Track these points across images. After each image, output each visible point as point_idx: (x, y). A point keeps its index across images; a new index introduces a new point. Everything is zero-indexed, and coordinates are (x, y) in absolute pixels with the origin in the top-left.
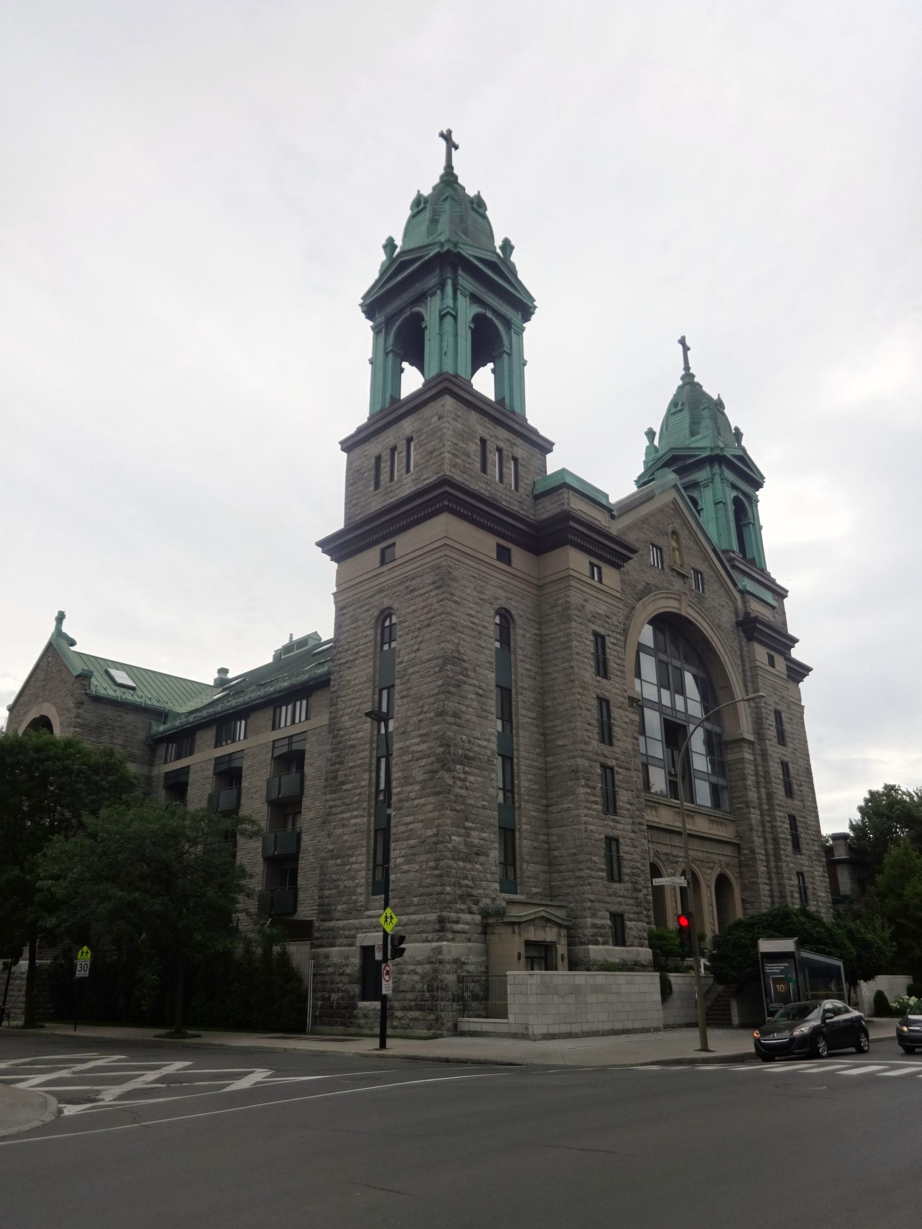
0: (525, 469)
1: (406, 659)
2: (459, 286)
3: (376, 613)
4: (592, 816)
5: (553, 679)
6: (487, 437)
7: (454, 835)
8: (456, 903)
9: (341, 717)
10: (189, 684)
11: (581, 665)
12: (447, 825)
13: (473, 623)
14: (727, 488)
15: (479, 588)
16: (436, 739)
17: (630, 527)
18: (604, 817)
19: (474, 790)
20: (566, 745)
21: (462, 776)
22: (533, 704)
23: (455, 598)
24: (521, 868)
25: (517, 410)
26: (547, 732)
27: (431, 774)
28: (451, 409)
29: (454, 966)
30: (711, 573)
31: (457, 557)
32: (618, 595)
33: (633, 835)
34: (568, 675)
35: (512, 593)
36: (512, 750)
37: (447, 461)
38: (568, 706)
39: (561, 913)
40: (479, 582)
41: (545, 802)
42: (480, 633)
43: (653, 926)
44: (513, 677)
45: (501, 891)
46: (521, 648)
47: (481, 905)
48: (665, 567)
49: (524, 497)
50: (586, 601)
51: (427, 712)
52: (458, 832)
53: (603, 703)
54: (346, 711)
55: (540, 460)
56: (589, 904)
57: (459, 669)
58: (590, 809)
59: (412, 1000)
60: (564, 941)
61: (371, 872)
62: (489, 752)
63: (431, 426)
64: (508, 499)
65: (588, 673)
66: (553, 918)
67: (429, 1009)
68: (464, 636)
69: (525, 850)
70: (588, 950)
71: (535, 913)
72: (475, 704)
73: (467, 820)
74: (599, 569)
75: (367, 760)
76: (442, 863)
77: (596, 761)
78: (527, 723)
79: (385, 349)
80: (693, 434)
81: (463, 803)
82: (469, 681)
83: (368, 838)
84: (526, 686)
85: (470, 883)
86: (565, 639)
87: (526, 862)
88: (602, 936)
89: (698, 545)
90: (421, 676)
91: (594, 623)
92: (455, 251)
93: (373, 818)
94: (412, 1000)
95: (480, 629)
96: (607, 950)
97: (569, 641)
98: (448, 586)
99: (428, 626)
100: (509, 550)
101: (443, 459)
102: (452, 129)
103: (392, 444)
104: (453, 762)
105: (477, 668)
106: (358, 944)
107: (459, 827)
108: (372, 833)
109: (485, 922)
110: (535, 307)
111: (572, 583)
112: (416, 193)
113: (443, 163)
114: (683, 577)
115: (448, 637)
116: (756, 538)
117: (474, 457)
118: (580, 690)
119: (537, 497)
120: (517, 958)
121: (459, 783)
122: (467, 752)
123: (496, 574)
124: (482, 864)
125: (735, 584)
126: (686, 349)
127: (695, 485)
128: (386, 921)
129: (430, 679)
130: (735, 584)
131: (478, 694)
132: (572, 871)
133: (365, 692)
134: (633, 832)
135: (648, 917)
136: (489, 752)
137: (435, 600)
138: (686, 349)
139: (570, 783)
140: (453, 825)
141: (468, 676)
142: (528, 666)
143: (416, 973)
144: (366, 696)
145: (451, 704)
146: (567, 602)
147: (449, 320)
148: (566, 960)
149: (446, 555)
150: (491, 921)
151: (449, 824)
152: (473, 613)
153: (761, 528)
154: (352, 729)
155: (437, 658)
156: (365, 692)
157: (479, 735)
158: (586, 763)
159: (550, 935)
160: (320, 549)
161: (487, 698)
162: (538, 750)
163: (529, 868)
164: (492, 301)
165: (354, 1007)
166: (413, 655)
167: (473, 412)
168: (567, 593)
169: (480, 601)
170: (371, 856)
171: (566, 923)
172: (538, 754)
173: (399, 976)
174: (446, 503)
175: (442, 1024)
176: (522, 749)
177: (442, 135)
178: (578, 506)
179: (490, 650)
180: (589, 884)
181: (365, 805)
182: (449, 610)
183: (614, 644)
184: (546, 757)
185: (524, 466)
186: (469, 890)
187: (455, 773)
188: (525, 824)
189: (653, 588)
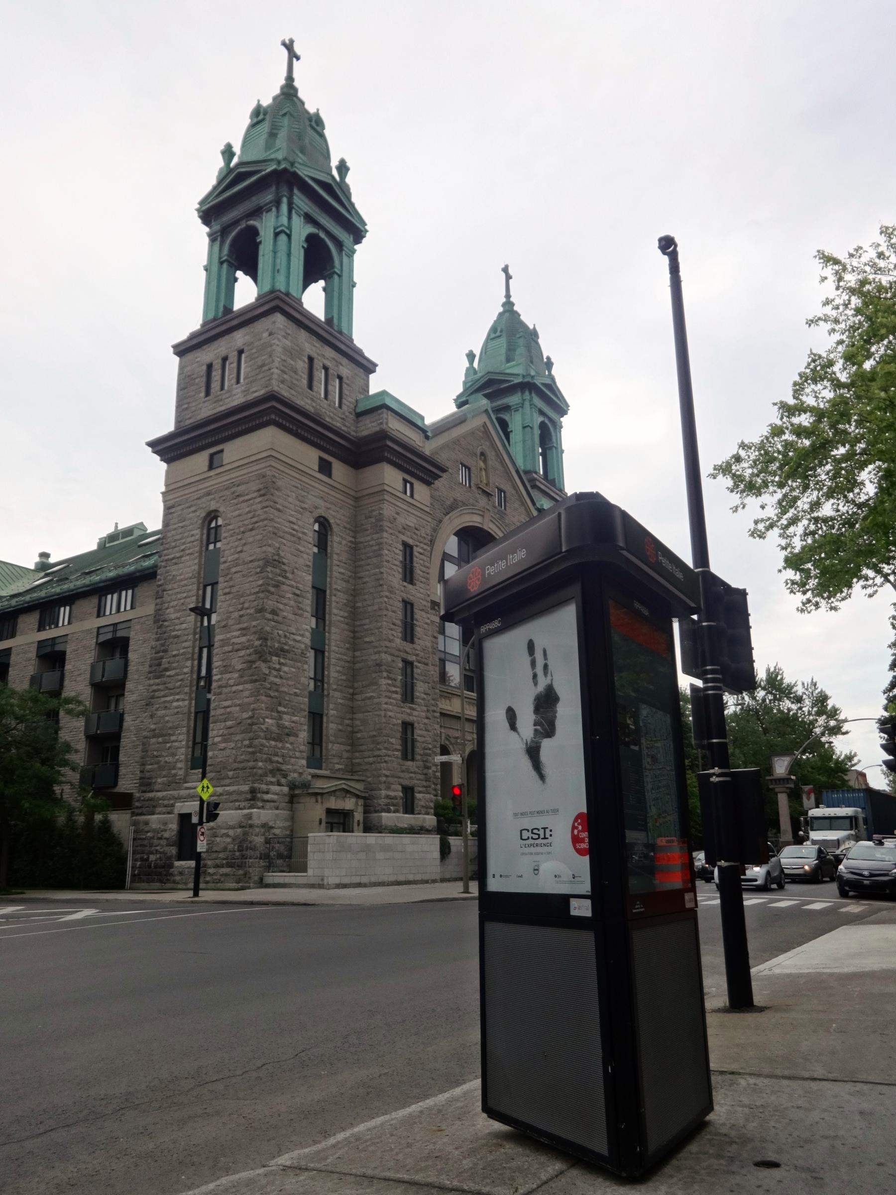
0: (349, 388)
1: (230, 559)
2: (294, 206)
3: (203, 515)
4: (391, 704)
5: (364, 583)
6: (314, 355)
7: (267, 718)
8: (267, 776)
9: (167, 608)
11: (389, 571)
12: (262, 709)
14: (534, 414)
15: (300, 498)
16: (255, 633)
17: (442, 448)
18: (402, 705)
19: (287, 679)
20: (372, 642)
21: (278, 666)
22: (345, 604)
23: (278, 506)
24: (327, 746)
25: (345, 330)
28: (282, 327)
29: (263, 830)
30: (514, 492)
31: (282, 468)
32: (428, 509)
33: (426, 721)
34: (378, 580)
36: (325, 644)
37: (275, 376)
38: (375, 607)
39: (360, 786)
40: (301, 492)
41: (351, 691)
42: (299, 538)
43: (440, 798)
44: (328, 579)
45: (308, 767)
46: (337, 554)
47: (289, 778)
48: (472, 484)
49: (347, 414)
50: (398, 514)
51: (247, 609)
52: (271, 715)
53: (408, 606)
54: (172, 604)
55: (363, 379)
56: (384, 779)
57: (278, 571)
58: (390, 698)
59: (224, 859)
60: (360, 809)
61: (190, 750)
62: (303, 646)
63: (262, 342)
64: (332, 415)
65: (394, 577)
66: (352, 790)
67: (238, 866)
68: (285, 542)
69: (331, 732)
70: (381, 817)
71: (336, 785)
73: (280, 705)
75: (190, 650)
76: (256, 742)
77: (397, 656)
78: (338, 621)
79: (220, 258)
80: (508, 360)
81: (277, 691)
82: (288, 582)
83: (189, 719)
84: (339, 588)
85: (280, 760)
86: (376, 548)
87: (331, 742)
88: (394, 805)
89: (503, 467)
90: (244, 576)
91: (403, 534)
92: (292, 170)
93: (193, 702)
94: (224, 859)
95: (300, 535)
96: (398, 818)
97: (381, 549)
98: (272, 495)
99: (252, 530)
100: (330, 464)
101: (272, 374)
102: (294, 39)
103: (223, 354)
104: (270, 653)
105: (295, 571)
106: (176, 811)
107: (272, 711)
108: (193, 715)
109: (292, 793)
110: (367, 231)
111: (386, 497)
112: (256, 102)
113: (284, 73)
114: (488, 495)
115: (270, 542)
118: (387, 594)
119: (359, 415)
120: (318, 823)
122: (283, 646)
123: (317, 485)
124: (292, 744)
125: (534, 503)
126: (508, 277)
127: (507, 408)
128: (203, 790)
129: (251, 579)
130: (534, 503)
131: (295, 594)
132: (372, 750)
133: (190, 587)
134: (427, 718)
135: (435, 790)
136: (303, 646)
137: (259, 506)
138: (508, 277)
139: (374, 675)
141: (286, 578)
142: (342, 571)
143: (228, 836)
144: (190, 591)
145: (270, 602)
147: (283, 238)
148: (361, 825)
149: (271, 466)
150: (297, 792)
151: (264, 708)
153: (562, 451)
154: (176, 621)
156: (190, 587)
157: (294, 631)
158: (389, 658)
159: (348, 804)
160: (150, 449)
161: (304, 597)
162: (347, 645)
163: (334, 748)
164: (325, 222)
165: (171, 866)
166: (236, 556)
167: (302, 331)
168: (381, 506)
169: (301, 510)
170: (191, 735)
171: (363, 795)
172: (348, 649)
173: (213, 839)
174: (273, 417)
176: (333, 644)
177: (284, 44)
178: (395, 426)
179: (308, 554)
180: (385, 762)
181: (187, 690)
182: (272, 516)
183: (421, 554)
185: (348, 385)
186: (279, 765)
187: (271, 664)
188: (332, 710)
189: (460, 504)
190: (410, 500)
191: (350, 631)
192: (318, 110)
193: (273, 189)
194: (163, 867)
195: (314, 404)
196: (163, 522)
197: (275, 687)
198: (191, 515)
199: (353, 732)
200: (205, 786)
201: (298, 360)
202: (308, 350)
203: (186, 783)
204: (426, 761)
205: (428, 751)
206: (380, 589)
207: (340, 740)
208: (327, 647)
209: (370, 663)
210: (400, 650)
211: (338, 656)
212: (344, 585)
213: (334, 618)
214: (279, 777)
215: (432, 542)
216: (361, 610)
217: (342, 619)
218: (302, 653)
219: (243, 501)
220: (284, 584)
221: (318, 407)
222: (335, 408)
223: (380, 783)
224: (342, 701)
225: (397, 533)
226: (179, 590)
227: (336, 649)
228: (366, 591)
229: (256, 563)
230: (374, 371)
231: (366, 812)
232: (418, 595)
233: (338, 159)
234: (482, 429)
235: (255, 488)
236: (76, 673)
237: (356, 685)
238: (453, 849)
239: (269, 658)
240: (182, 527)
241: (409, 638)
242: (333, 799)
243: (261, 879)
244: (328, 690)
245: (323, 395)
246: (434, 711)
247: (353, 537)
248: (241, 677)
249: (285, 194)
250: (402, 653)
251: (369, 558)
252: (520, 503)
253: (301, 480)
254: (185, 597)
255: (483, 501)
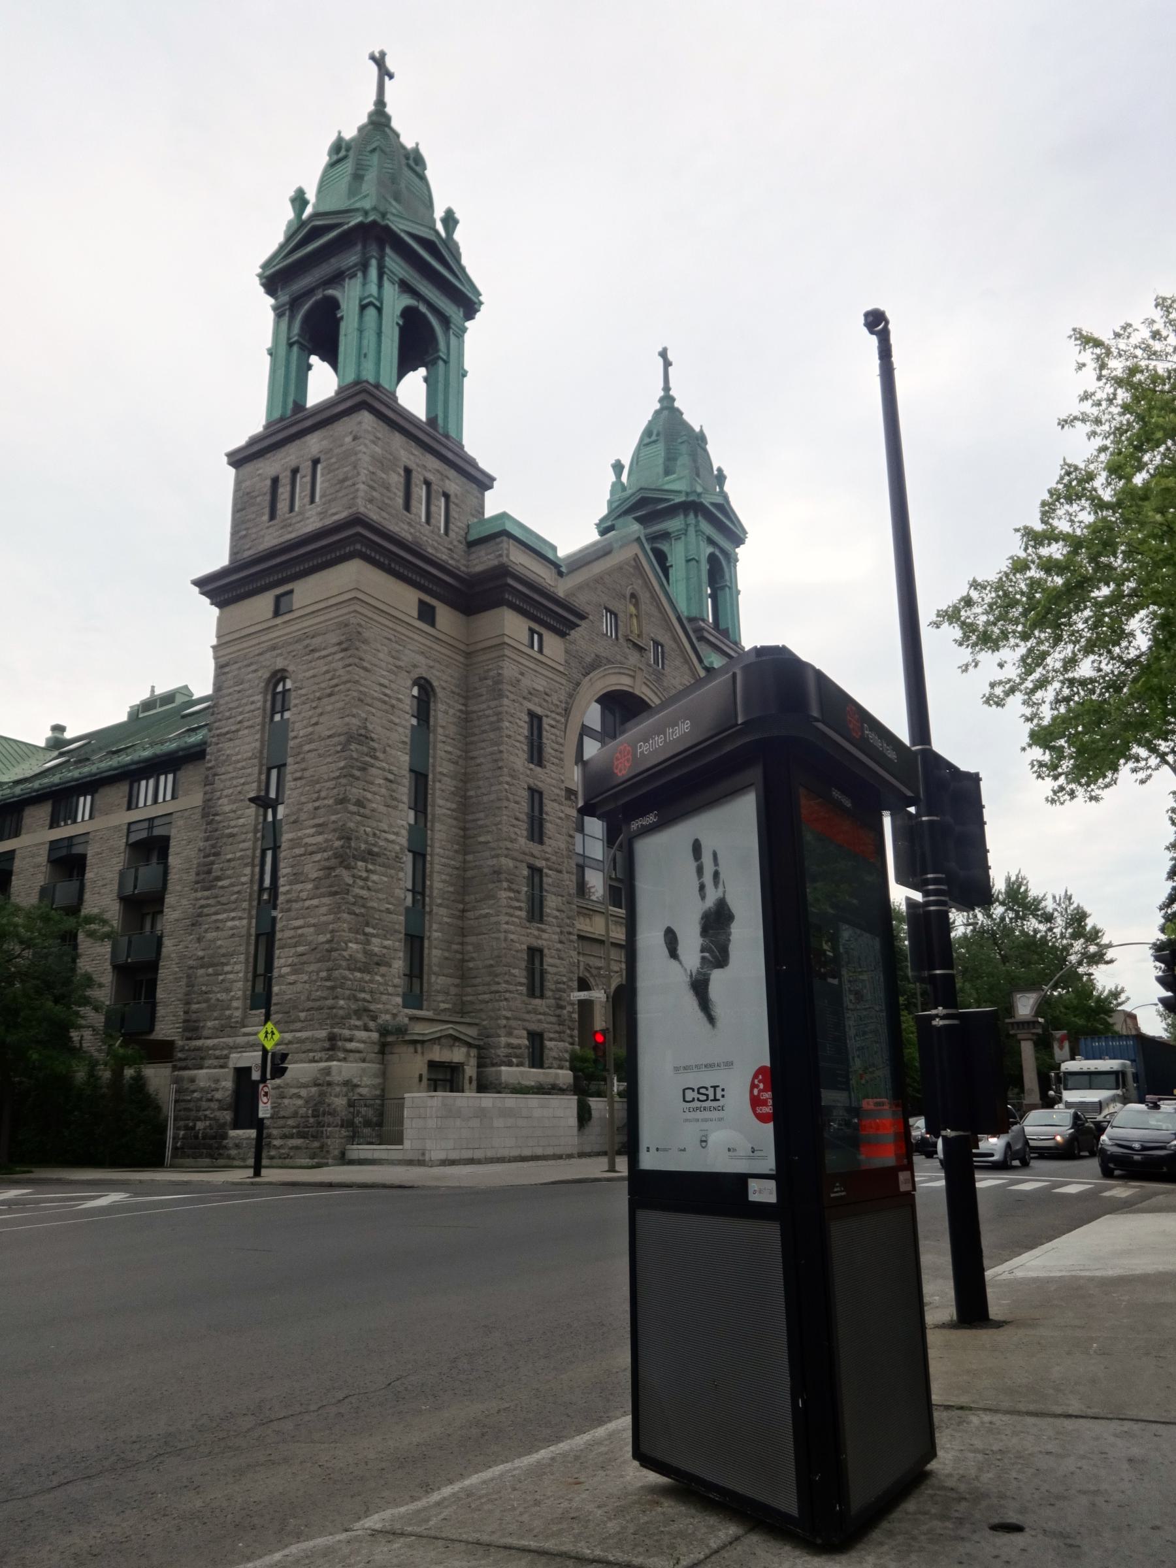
0: (458, 510)
1: (301, 733)
2: (386, 270)
4: (513, 924)
5: (479, 765)
6: (412, 466)
7: (351, 942)
8: (350, 1018)
9: (219, 798)
10: (23, 747)
12: (344, 931)
13: (386, 695)
15: (394, 653)
16: (335, 830)
17: (580, 587)
18: (528, 924)
19: (376, 891)
21: (364, 874)
22: (452, 793)
23: (365, 664)
24: (429, 979)
25: (453, 434)
26: (467, 826)
27: (327, 872)
28: (370, 429)
29: (345, 1089)
30: (674, 646)
31: (370, 614)
32: (561, 669)
34: (496, 761)
35: (434, 660)
36: (426, 846)
37: (361, 494)
38: (493, 797)
39: (472, 1032)
40: (394, 645)
41: (461, 906)
42: (393, 706)
43: (577, 1047)
44: (431, 760)
45: (405, 1006)
46: (443, 727)
47: (380, 1021)
49: (456, 543)
50: (522, 674)
51: (324, 798)
52: (356, 939)
53: (536, 795)
54: (225, 792)
55: (477, 497)
56: (504, 1022)
57: (365, 749)
58: (511, 916)
59: (294, 1127)
60: (473, 1062)
61: (250, 984)
62: (397, 848)
63: (344, 448)
64: (436, 545)
65: (518, 758)
66: (462, 1037)
67: (313, 1136)
68: (374, 711)
69: (435, 960)
70: (500, 1071)
71: (441, 1030)
72: (383, 791)
73: (367, 925)
74: (540, 636)
75: (249, 853)
76: (336, 973)
77: (522, 861)
78: (444, 815)
79: (289, 339)
80: (667, 472)
81: (364, 906)
82: (378, 764)
83: (248, 944)
84: (445, 771)
85: (368, 997)
86: (493, 719)
87: (435, 974)
88: (517, 1057)
89: (660, 612)
90: (320, 756)
91: (530, 701)
92: (383, 223)
93: (254, 921)
95: (394, 702)
97: (500, 720)
98: (357, 649)
99: (330, 695)
100: (433, 608)
101: (357, 490)
102: (386, 51)
103: (293, 464)
105: (388, 749)
106: (231, 1065)
107: (357, 933)
108: (253, 938)
109: (382, 1040)
110: (481, 303)
111: (507, 652)
114: (641, 649)
115: (355, 711)
116: (732, 605)
117: (397, 491)
118: (508, 779)
119: (471, 544)
121: (361, 883)
122: (371, 847)
123: (416, 637)
124: (383, 976)
125: (700, 661)
126: (667, 364)
127: (665, 536)
128: (266, 1036)
129: (329, 760)
130: (700, 661)
131: (386, 779)
132: (488, 984)
133: (249, 771)
134: (561, 942)
136: (397, 848)
137: (340, 664)
138: (667, 364)
139: (491, 886)
140: (350, 929)
141: (376, 758)
142: (449, 749)
143: (299, 1097)
145: (354, 790)
146: (499, 674)
147: (371, 312)
148: (474, 1083)
149: (355, 611)
150: (390, 1039)
152: (386, 682)
153: (738, 592)
154: (232, 815)
155: (340, 735)
156: (249, 771)
157: (386, 828)
158: (511, 863)
159: (457, 1055)
160: (196, 589)
161: (399, 784)
162: (456, 847)
163: (439, 981)
165: (225, 1136)
166: (310, 729)
167: (397, 434)
168: (500, 664)
169: (395, 669)
170: (251, 964)
171: (477, 1043)
172: (456, 851)
173: (279, 1101)
174: (358, 547)
175: (328, 1152)
176: (437, 844)
177: (372, 57)
178: (519, 559)
179: (404, 727)
180: (506, 999)
181: (245, 905)
182: (357, 678)
184: (465, 854)
185: (456, 505)
186: (366, 1004)
187: (355, 871)
188: (436, 931)
189: (604, 661)
190: (539, 656)
191: (461, 829)
192: (417, 144)
193: (359, 248)
194: (214, 1138)
195: (412, 531)
196: (215, 684)
197: (360, 901)
198: (250, 676)
199: (463, 961)
200: (269, 1031)
201: (391, 472)
202: (404, 459)
203: (244, 1027)
204: (560, 999)
205: (562, 986)
206: (498, 773)
207: (446, 971)
208: (429, 849)
209: (486, 870)
210: (524, 853)
211: (443, 860)
212: (452, 767)
213: (438, 811)
214: (366, 1019)
215: (567, 712)
216: (474, 800)
217: (449, 812)
218: (397, 857)
219: (319, 658)
220: (372, 766)
221: (418, 534)
222: (439, 536)
223: (499, 1027)
224: (448, 920)
225: (521, 699)
226: (234, 774)
227: (441, 851)
228: (480, 775)
229: (336, 739)
230: (491, 487)
231: (480, 1065)
232: (549, 780)
233: (444, 209)
234: (633, 563)
235: (334, 641)
236: (100, 883)
237: (467, 898)
238: (595, 1114)
239: (353, 864)
240: (239, 692)
241: (536, 837)
242: (437, 1048)
243: (343, 1154)
244: (431, 906)
245: (423, 519)
246: (570, 933)
247: (463, 705)
248: (317, 888)
249: (375, 254)
250: (527, 857)
251: (484, 732)
252: (682, 660)
253: (395, 630)
254: (243, 784)
255: (634, 658)
